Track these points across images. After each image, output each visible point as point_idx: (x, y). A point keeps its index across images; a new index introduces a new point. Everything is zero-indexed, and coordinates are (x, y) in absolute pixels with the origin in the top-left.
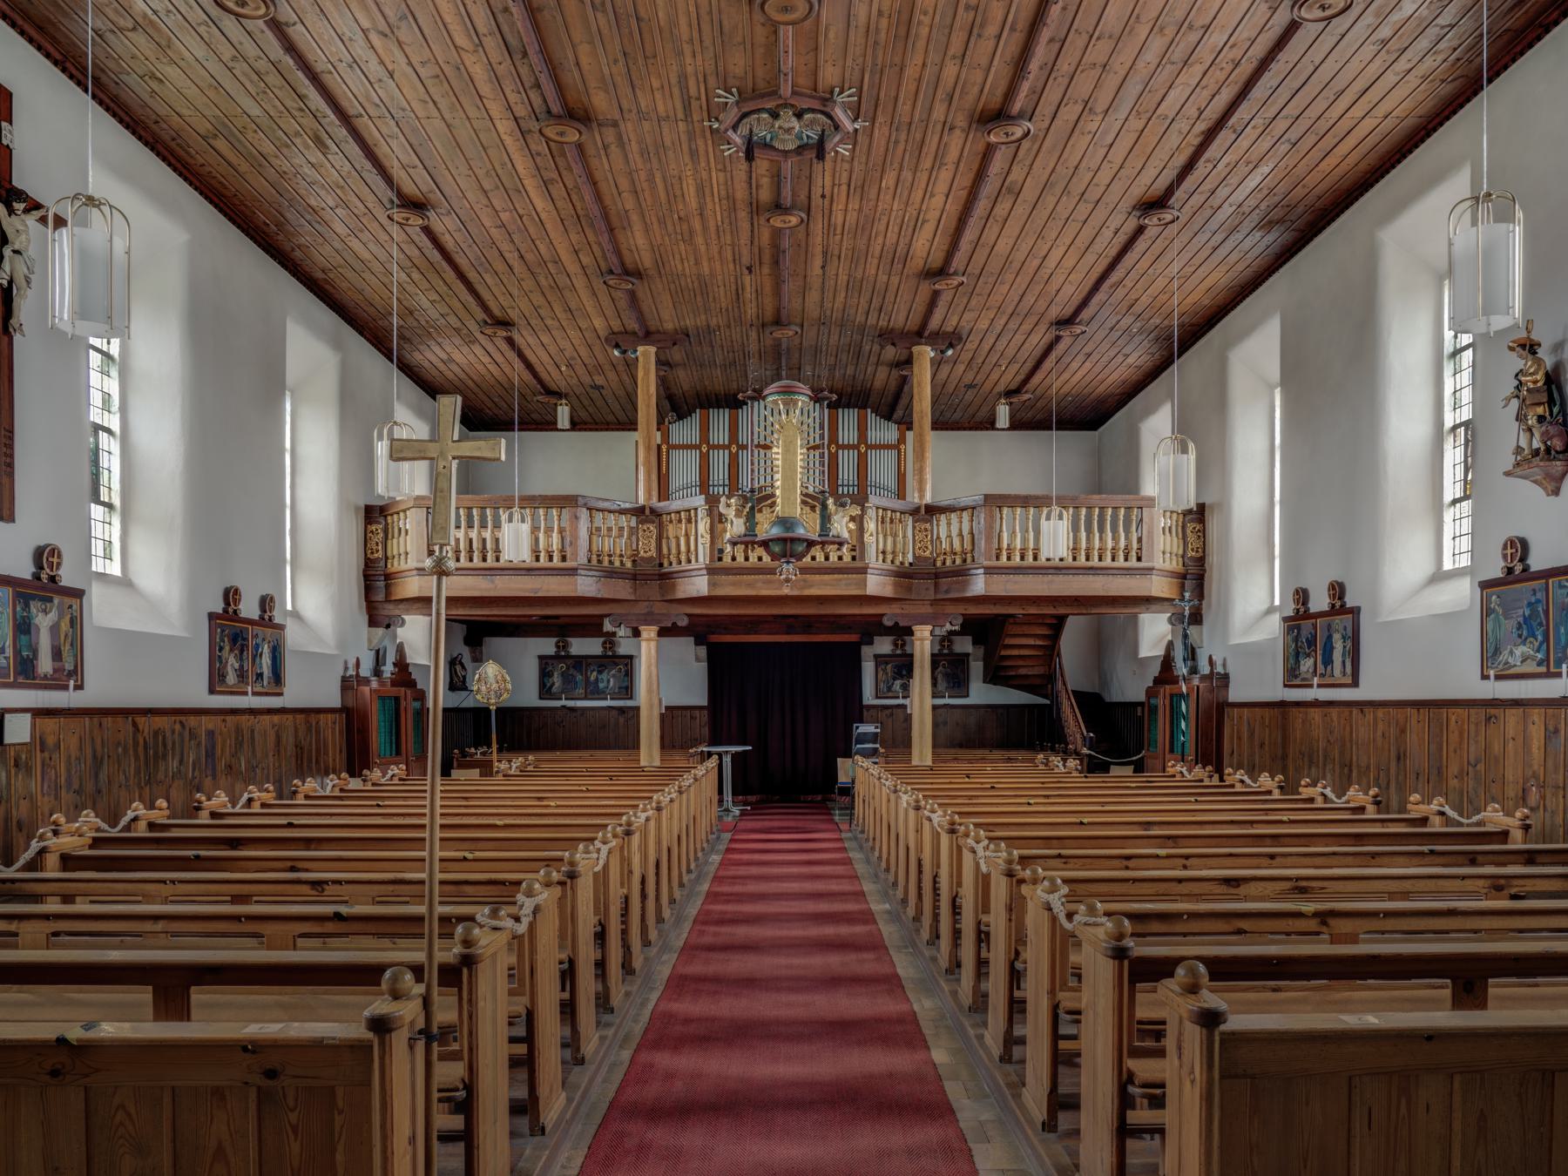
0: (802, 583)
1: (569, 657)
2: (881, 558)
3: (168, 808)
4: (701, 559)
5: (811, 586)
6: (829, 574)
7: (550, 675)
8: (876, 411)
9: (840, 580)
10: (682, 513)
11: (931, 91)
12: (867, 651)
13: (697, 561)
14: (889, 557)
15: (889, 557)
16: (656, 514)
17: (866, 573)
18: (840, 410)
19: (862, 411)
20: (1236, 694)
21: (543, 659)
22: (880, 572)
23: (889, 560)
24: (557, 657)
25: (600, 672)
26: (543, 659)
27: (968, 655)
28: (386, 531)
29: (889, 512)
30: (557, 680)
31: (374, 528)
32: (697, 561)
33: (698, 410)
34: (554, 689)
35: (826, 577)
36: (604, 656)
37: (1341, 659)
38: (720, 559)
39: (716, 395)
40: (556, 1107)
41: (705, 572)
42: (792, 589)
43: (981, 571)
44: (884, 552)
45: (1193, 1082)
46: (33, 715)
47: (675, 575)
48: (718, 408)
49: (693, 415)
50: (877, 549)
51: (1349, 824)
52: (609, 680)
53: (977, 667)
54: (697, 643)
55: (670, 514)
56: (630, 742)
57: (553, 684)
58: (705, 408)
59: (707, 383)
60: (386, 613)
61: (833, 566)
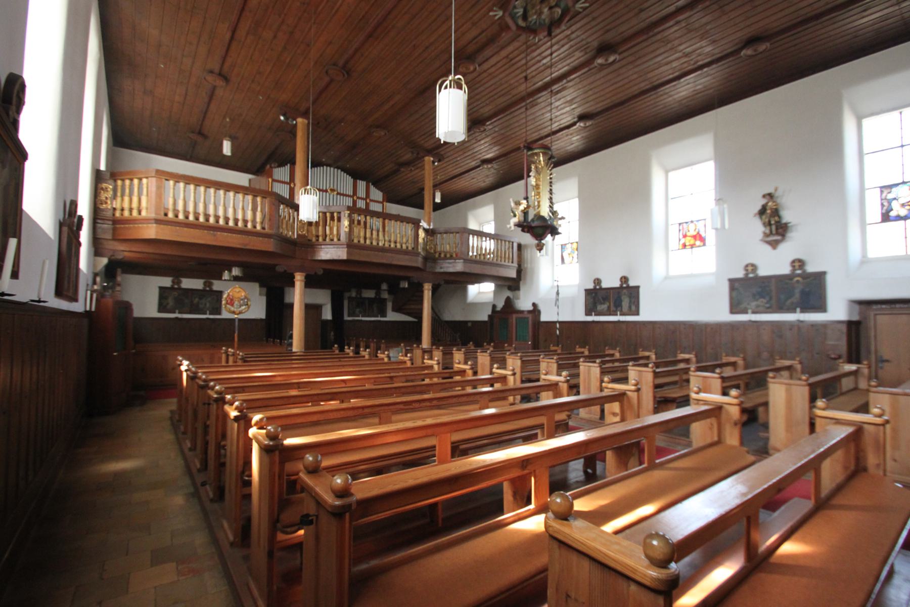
1: (180, 289)
3: (514, 396)
7: (166, 298)
8: (374, 184)
11: (884, 19)
12: (347, 295)
20: (544, 318)
21: (162, 290)
24: (172, 288)
25: (200, 299)
26: (162, 290)
27: (386, 299)
28: (115, 190)
30: (171, 302)
31: (104, 185)
33: (289, 165)
34: (168, 307)
36: (204, 290)
37: (628, 305)
41: (345, 246)
43: (462, 261)
46: (497, 286)
48: (317, 167)
49: (286, 166)
51: (284, 370)
52: (207, 302)
53: (389, 305)
54: (261, 286)
56: (417, 338)
57: (168, 304)
60: (111, 247)
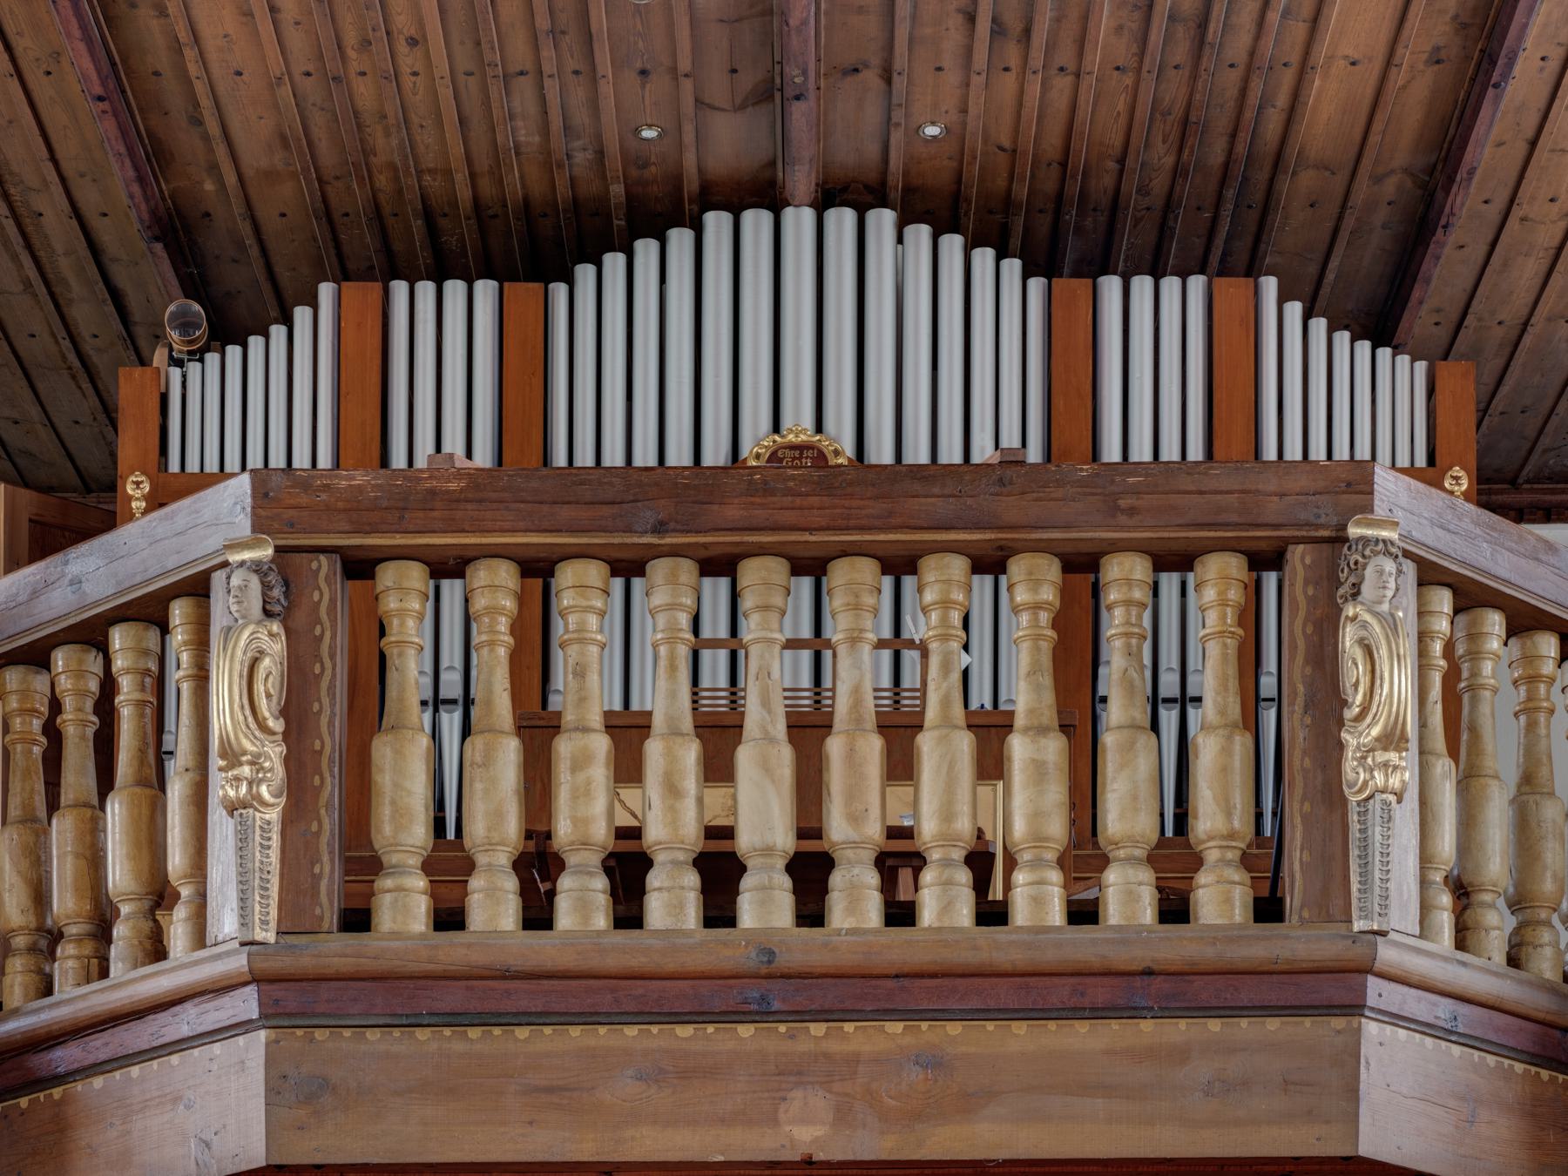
0: (915, 1075)
2: (1445, 920)
4: (225, 923)
5: (968, 1104)
6: (1098, 1013)
9: (1181, 1054)
10: (119, 638)
13: (200, 938)
14: (1497, 923)
15: (1497, 923)
16: (30, 773)
17: (1355, 1008)
18: (1111, 286)
19: (1232, 289)
22: (1442, 1010)
23: (1496, 944)
29: (1495, 622)
32: (200, 938)
33: (326, 291)
35: (1082, 1036)
38: (357, 919)
39: (428, 214)
40: (1498, 860)
42: (843, 1116)
44: (1462, 891)
45: (107, 1044)
47: (66, 1056)
50: (1426, 860)
55: (36, 656)
58: (366, 275)
59: (364, 92)
61: (1124, 957)
